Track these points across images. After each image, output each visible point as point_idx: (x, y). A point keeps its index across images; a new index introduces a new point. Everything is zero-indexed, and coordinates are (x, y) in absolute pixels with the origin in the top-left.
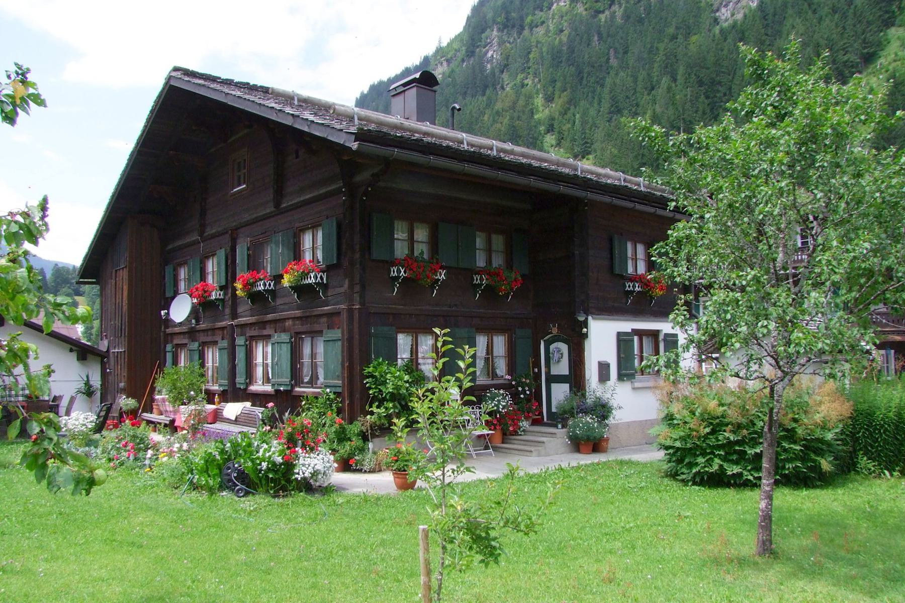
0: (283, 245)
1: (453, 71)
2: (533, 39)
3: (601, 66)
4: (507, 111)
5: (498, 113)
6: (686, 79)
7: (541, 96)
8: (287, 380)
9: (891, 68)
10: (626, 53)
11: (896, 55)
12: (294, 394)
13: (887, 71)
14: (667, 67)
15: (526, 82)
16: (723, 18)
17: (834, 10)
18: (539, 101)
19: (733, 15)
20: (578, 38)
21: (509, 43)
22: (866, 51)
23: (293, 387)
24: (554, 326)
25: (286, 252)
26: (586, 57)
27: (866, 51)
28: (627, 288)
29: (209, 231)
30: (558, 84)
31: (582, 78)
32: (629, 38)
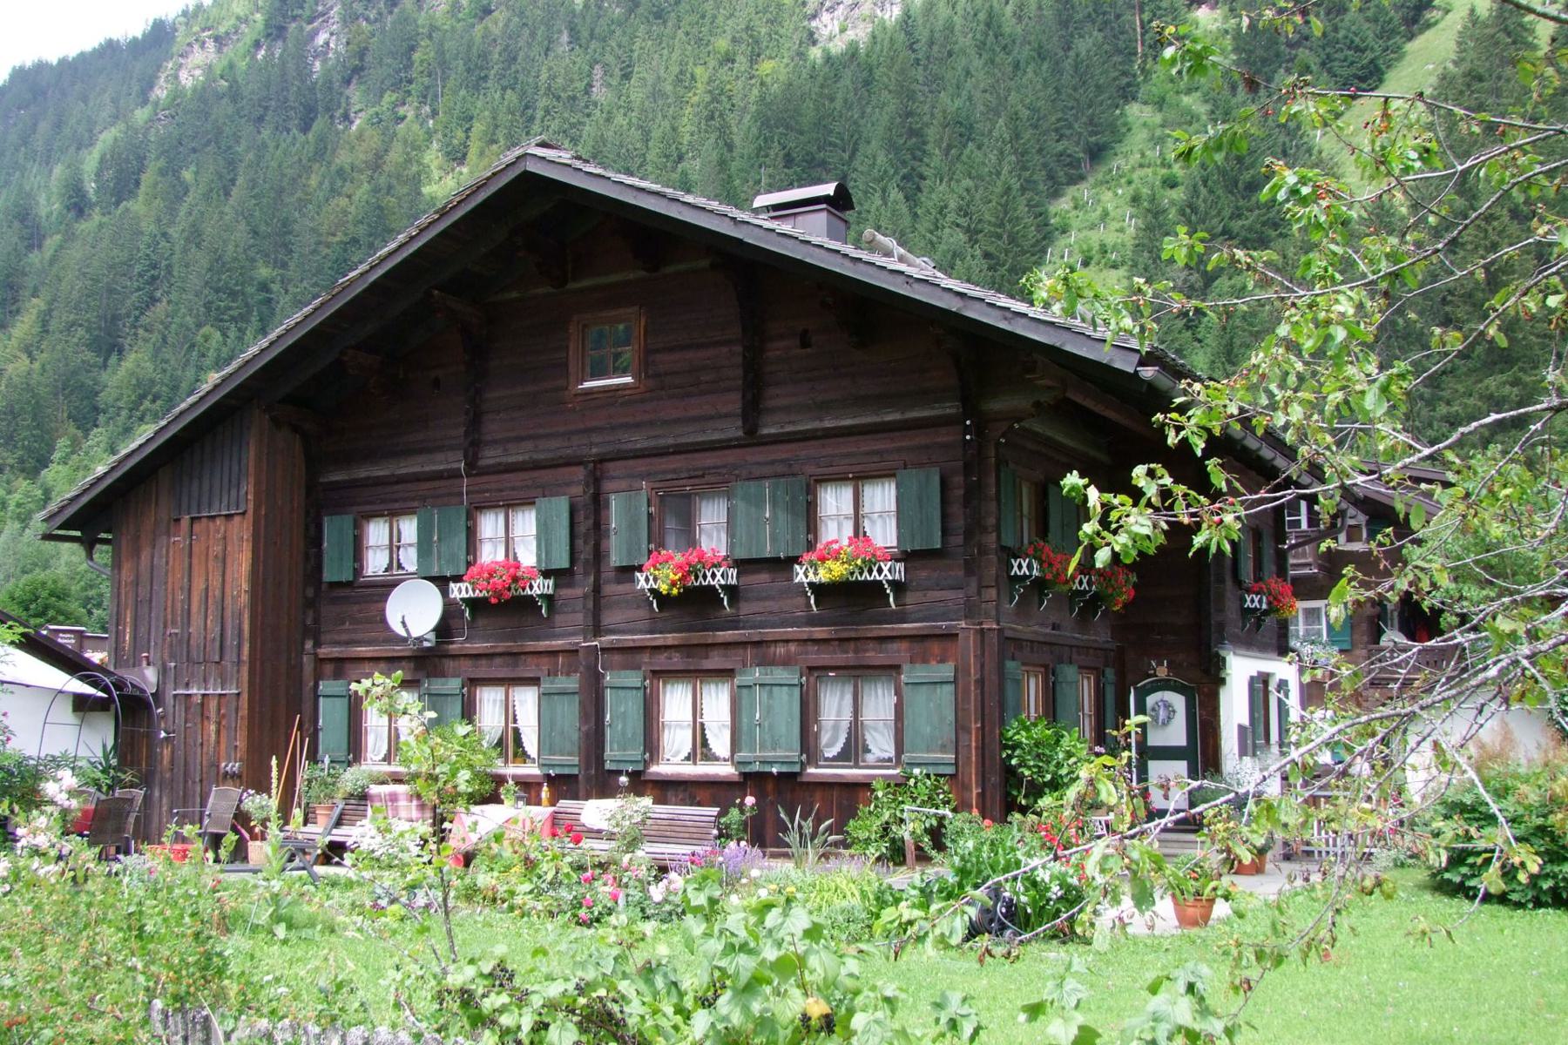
0: (774, 505)
1: (231, 66)
2: (422, 19)
3: (574, 98)
4: (361, 171)
5: (341, 172)
6: (760, 149)
7: (435, 145)
8: (794, 754)
9: (1135, 176)
10: (626, 76)
11: (1143, 155)
12: (805, 779)
13: (1130, 183)
14: (712, 118)
15: (401, 111)
16: (826, 32)
17: (1041, 54)
18: (433, 157)
19: (843, 30)
20: (526, 32)
21: (367, 19)
22: (1093, 139)
23: (647, 764)
24: (1160, 664)
25: (782, 516)
26: (544, 76)
27: (1093, 139)
28: (1248, 604)
29: (490, 456)
30: (478, 127)
31: (532, 119)
32: (636, 47)
